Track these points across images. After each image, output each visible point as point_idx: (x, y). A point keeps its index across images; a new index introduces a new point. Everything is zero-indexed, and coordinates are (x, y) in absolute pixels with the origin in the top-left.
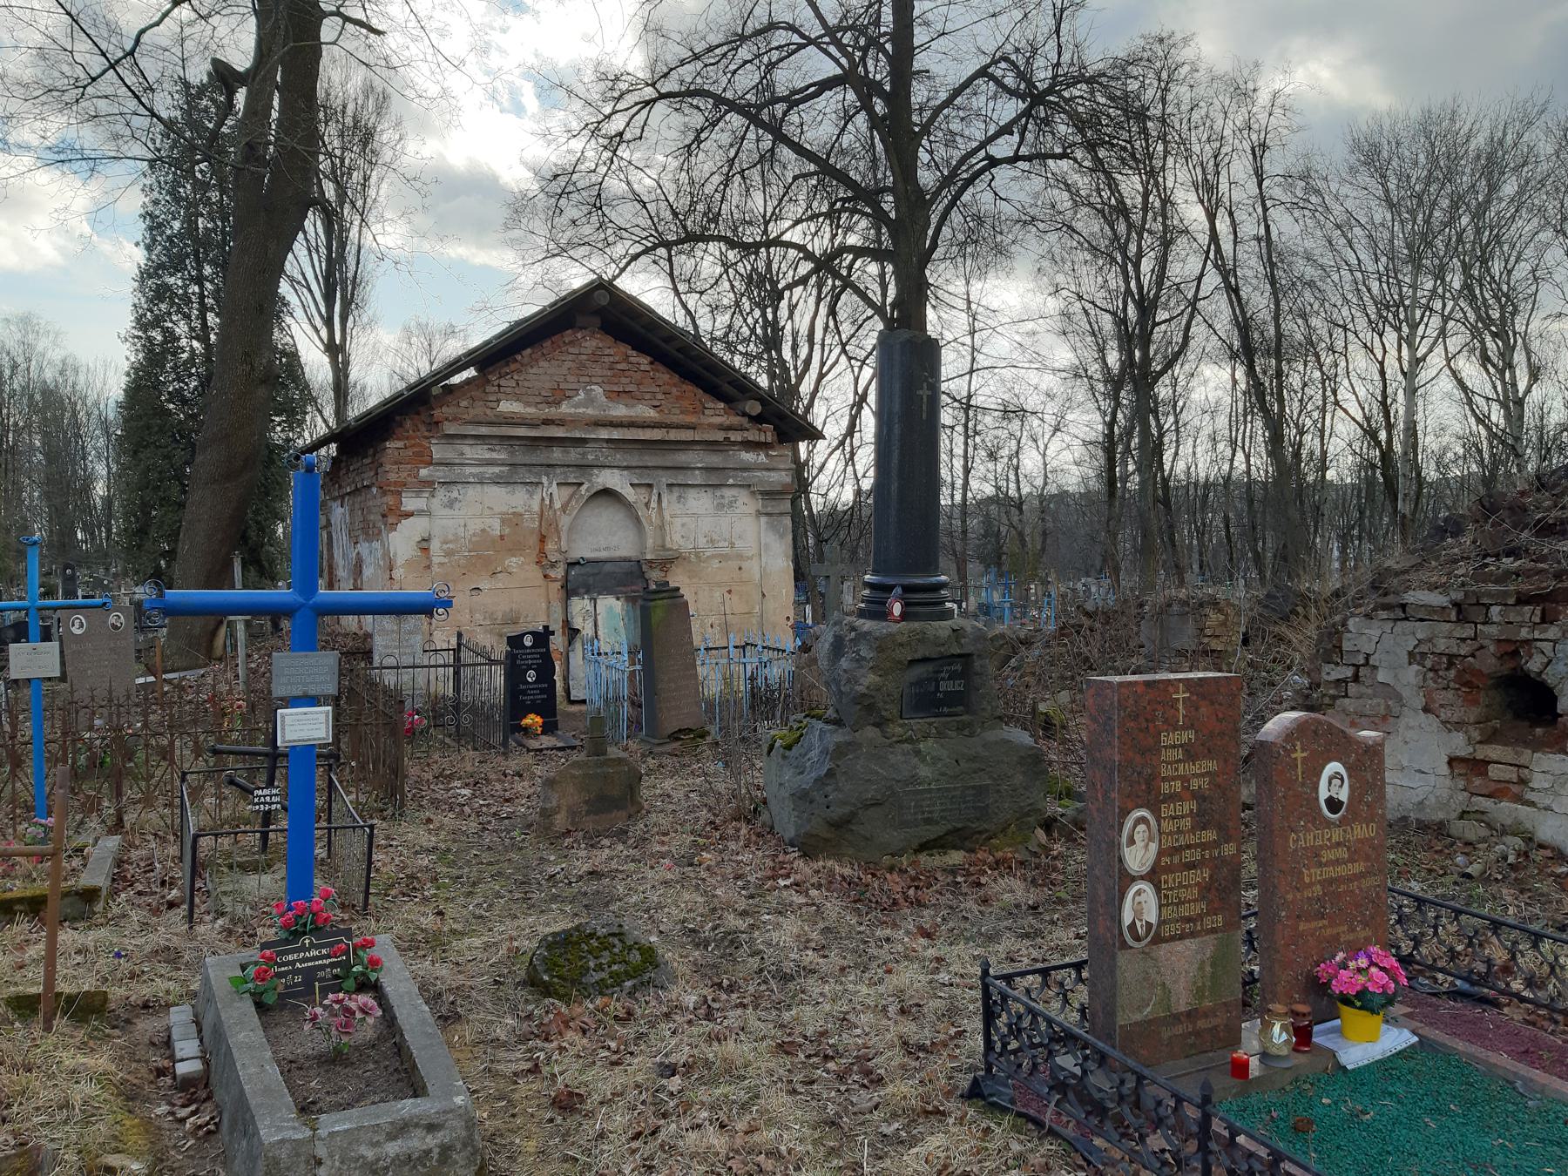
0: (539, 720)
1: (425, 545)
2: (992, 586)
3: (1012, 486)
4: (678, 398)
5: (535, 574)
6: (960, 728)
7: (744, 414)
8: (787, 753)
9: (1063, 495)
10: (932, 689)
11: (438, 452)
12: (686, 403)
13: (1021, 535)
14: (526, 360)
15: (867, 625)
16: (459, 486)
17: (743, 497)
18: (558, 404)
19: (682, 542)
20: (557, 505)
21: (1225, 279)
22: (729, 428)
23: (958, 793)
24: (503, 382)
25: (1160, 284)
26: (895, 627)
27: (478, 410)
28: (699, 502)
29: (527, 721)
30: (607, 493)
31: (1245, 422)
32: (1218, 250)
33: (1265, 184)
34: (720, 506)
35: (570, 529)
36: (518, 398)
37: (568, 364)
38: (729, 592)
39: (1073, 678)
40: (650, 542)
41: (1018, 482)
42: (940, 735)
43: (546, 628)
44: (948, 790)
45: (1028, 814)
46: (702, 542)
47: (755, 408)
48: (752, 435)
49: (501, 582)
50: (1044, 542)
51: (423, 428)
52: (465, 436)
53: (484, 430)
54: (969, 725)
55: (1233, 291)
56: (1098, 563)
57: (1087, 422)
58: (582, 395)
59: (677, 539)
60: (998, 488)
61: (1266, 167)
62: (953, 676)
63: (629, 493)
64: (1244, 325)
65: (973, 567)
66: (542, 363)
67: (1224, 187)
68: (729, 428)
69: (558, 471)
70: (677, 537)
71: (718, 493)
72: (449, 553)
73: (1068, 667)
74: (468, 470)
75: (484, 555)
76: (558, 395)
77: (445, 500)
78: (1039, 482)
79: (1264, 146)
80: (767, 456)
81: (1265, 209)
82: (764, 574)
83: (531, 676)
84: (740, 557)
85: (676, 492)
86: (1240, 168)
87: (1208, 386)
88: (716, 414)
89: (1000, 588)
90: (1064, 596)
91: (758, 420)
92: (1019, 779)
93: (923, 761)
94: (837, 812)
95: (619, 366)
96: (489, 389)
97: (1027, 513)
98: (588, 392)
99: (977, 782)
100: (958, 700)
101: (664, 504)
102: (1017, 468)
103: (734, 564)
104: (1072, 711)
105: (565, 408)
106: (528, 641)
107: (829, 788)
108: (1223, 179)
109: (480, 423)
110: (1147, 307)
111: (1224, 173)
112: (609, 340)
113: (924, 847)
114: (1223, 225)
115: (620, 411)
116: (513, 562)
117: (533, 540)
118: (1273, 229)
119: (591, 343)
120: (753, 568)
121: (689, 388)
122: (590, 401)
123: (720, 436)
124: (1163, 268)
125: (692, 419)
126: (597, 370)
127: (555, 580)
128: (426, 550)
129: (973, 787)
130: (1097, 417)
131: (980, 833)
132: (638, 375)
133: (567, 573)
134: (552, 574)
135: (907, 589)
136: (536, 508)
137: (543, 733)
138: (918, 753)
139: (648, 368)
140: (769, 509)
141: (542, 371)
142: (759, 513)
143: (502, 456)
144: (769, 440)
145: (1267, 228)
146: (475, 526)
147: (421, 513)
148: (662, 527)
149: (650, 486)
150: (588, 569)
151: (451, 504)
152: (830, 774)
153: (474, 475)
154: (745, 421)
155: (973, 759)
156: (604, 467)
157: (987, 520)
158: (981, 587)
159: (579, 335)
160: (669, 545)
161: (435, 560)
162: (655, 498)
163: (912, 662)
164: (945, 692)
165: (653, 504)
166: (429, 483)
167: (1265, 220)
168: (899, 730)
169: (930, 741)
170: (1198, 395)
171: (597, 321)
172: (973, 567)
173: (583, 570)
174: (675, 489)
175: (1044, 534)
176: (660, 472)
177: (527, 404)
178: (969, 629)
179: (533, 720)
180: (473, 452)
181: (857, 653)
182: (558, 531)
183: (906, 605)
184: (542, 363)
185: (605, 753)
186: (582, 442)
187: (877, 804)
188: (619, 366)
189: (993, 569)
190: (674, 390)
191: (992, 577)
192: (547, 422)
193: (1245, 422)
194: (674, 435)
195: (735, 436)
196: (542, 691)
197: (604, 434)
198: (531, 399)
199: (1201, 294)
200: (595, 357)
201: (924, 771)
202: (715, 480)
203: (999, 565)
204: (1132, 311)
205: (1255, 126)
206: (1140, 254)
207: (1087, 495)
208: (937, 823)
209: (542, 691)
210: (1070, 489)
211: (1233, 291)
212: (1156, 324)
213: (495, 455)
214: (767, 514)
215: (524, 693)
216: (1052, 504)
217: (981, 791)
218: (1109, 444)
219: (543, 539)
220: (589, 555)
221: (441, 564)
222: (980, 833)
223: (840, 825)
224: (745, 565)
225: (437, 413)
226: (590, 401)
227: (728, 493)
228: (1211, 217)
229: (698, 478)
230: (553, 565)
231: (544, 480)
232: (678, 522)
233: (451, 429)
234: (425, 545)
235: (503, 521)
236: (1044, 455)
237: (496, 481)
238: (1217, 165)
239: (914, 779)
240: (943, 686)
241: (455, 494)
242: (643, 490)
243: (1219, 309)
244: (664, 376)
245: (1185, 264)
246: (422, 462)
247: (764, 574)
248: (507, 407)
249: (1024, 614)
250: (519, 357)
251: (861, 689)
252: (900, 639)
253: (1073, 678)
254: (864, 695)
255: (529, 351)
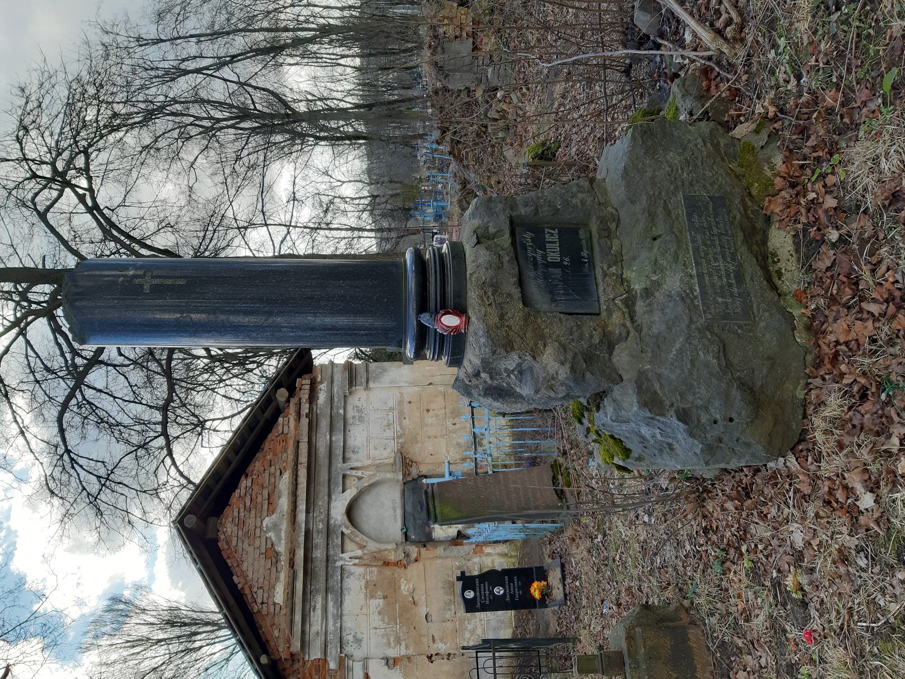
0: (535, 585)
1: (391, 662)
2: (423, 213)
3: (362, 201)
4: (275, 455)
5: (414, 570)
6: (607, 234)
7: (288, 401)
8: (635, 454)
9: (369, 171)
10: (557, 272)
11: (315, 654)
12: (279, 448)
13: (392, 196)
14: (242, 581)
15: (472, 358)
16: (344, 634)
17: (353, 401)
18: (277, 554)
19: (389, 450)
20: (359, 553)
21: (225, 64)
22: (299, 415)
23: (699, 237)
24: (259, 601)
25: (231, 106)
26: (476, 325)
27: (282, 621)
28: (357, 436)
29: (537, 595)
30: (350, 512)
31: (321, 58)
32: (207, 68)
33: (163, 38)
34: (361, 419)
35: (378, 541)
36: (272, 587)
37: (246, 546)
38: (428, 411)
39: (493, 146)
40: (389, 476)
41: (360, 198)
42: (618, 260)
43: (458, 579)
44: (696, 251)
45: (716, 146)
46: (389, 433)
47: (282, 394)
48: (305, 395)
49: (420, 597)
50: (396, 182)
51: (297, 666)
52: (303, 632)
53: (298, 617)
54: (603, 220)
55: (234, 58)
56: (407, 150)
57: (322, 155)
58: (271, 534)
59: (386, 453)
60: (364, 210)
61: (152, 37)
62: (541, 244)
63: (350, 493)
64: (258, 51)
65: (411, 224)
66: (244, 568)
67: (166, 65)
68: (299, 415)
69: (332, 552)
70: (385, 453)
71: (351, 421)
72: (398, 641)
73: (484, 150)
74: (331, 628)
75: (400, 611)
76: (271, 555)
77: (355, 646)
78: (360, 185)
79: (138, 39)
80: (321, 382)
81: (180, 38)
82: (413, 384)
83: (499, 591)
84: (401, 403)
85: (349, 455)
86: (153, 53)
87: (299, 80)
88: (287, 424)
89: (424, 208)
90: (429, 168)
91: (292, 391)
92: (673, 157)
93: (658, 284)
94: (740, 407)
95: (248, 504)
96: (264, 612)
97: (379, 192)
98: (269, 529)
99: (682, 211)
100: (571, 238)
101: (358, 464)
102: (352, 199)
103: (406, 406)
104: (521, 145)
105: (282, 548)
106: (470, 595)
107: (704, 419)
108: (161, 65)
109: (292, 621)
110: (244, 114)
111: (156, 64)
112: (227, 510)
113: (771, 279)
114: (191, 65)
115: (284, 503)
116: (405, 588)
117: (387, 571)
118: (194, 32)
119: (228, 528)
120: (410, 392)
121: (267, 445)
122: (275, 527)
123: (305, 421)
124: (221, 104)
125: (291, 442)
126: (251, 522)
127: (419, 553)
128: (396, 661)
129: (690, 216)
130: (318, 149)
131: (746, 208)
132: (256, 488)
133: (414, 542)
134: (414, 555)
135: (423, 307)
136: (361, 570)
137: (546, 579)
138: (648, 293)
139: (250, 480)
140: (364, 380)
141: (251, 568)
142: (367, 388)
143: (319, 600)
144: (308, 382)
145: (192, 36)
146: (376, 620)
147: (365, 667)
148: (378, 466)
149: (344, 476)
150: (410, 524)
151: (358, 641)
152: (684, 416)
153: (335, 623)
154: (293, 401)
155: (652, 217)
156: (328, 515)
157: (383, 215)
158: (423, 220)
159: (222, 537)
160: (392, 460)
161: (403, 652)
162: (354, 472)
163: (526, 301)
164: (562, 254)
165: (359, 473)
166: (341, 662)
167: (186, 37)
168: (616, 318)
169: (627, 274)
170: (306, 86)
171: (212, 520)
172: (411, 224)
173: (411, 529)
174: (347, 455)
175: (391, 182)
176: (333, 468)
177: (277, 579)
178: (476, 222)
179: (536, 590)
180: (316, 624)
181: (509, 372)
182: (380, 551)
183: (444, 308)
184: (244, 568)
185: (620, 654)
186: (308, 534)
187: (724, 350)
188: (248, 504)
189: (412, 212)
190: (268, 457)
191: (417, 213)
192: (292, 564)
193: (321, 58)
194: (303, 459)
195: (305, 408)
196: (511, 580)
197: (301, 517)
198: (273, 576)
199: (236, 79)
200: (240, 523)
201: (674, 282)
202: (340, 423)
203: (409, 209)
204: (246, 124)
205: (126, 44)
206: (211, 118)
207: (370, 155)
208: (740, 265)
209: (511, 580)
210: (365, 167)
211: (234, 58)
212: (255, 109)
213: (319, 606)
214: (367, 382)
215: (512, 596)
216: (374, 177)
217: (693, 206)
218: (335, 139)
219: (387, 564)
220: (399, 524)
221: (407, 647)
222: (746, 208)
223: (756, 399)
224: (407, 399)
225: (284, 656)
226: (275, 527)
227: (351, 413)
228: (186, 72)
229: (338, 438)
230: (407, 555)
231: (339, 564)
232: (373, 453)
233: (296, 646)
234: (391, 662)
235: (373, 596)
236: (344, 182)
237: (340, 604)
238: (152, 69)
239: (686, 297)
240: (554, 255)
241: (350, 638)
242: (348, 482)
243: (246, 68)
244: (257, 465)
245: (218, 90)
246: (324, 667)
247: (413, 384)
248: (279, 597)
249: (441, 193)
250: (240, 586)
251: (563, 373)
252: (494, 319)
253: (493, 146)
254: (573, 369)
255: (235, 578)
